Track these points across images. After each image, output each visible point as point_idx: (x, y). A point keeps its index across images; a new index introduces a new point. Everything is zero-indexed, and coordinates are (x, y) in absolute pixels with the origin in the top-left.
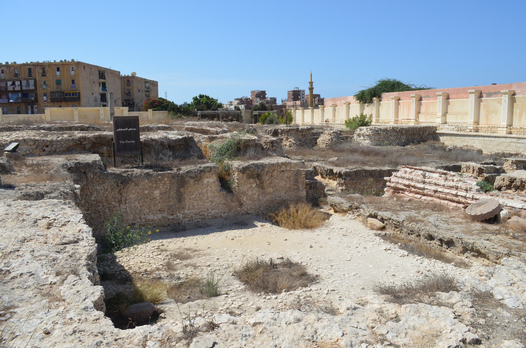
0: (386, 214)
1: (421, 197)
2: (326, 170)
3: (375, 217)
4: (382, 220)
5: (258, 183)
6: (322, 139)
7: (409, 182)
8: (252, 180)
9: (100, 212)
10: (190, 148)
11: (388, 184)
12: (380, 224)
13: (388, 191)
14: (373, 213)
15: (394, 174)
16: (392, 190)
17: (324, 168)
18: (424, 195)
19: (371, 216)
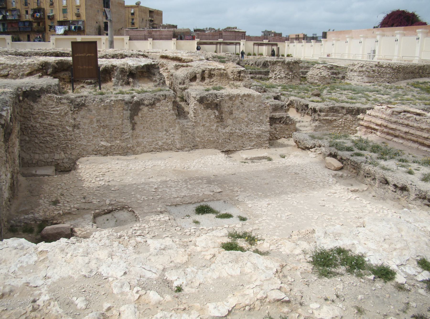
0: (346, 154)
1: (392, 139)
2: (302, 104)
3: (334, 156)
4: (341, 160)
5: (217, 113)
6: (311, 73)
7: (382, 122)
8: (209, 111)
9: (54, 136)
10: (152, 75)
11: (361, 122)
12: (339, 165)
13: (360, 130)
14: (333, 153)
15: (368, 112)
16: (364, 130)
17: (300, 102)
18: (396, 136)
19: (331, 155)
